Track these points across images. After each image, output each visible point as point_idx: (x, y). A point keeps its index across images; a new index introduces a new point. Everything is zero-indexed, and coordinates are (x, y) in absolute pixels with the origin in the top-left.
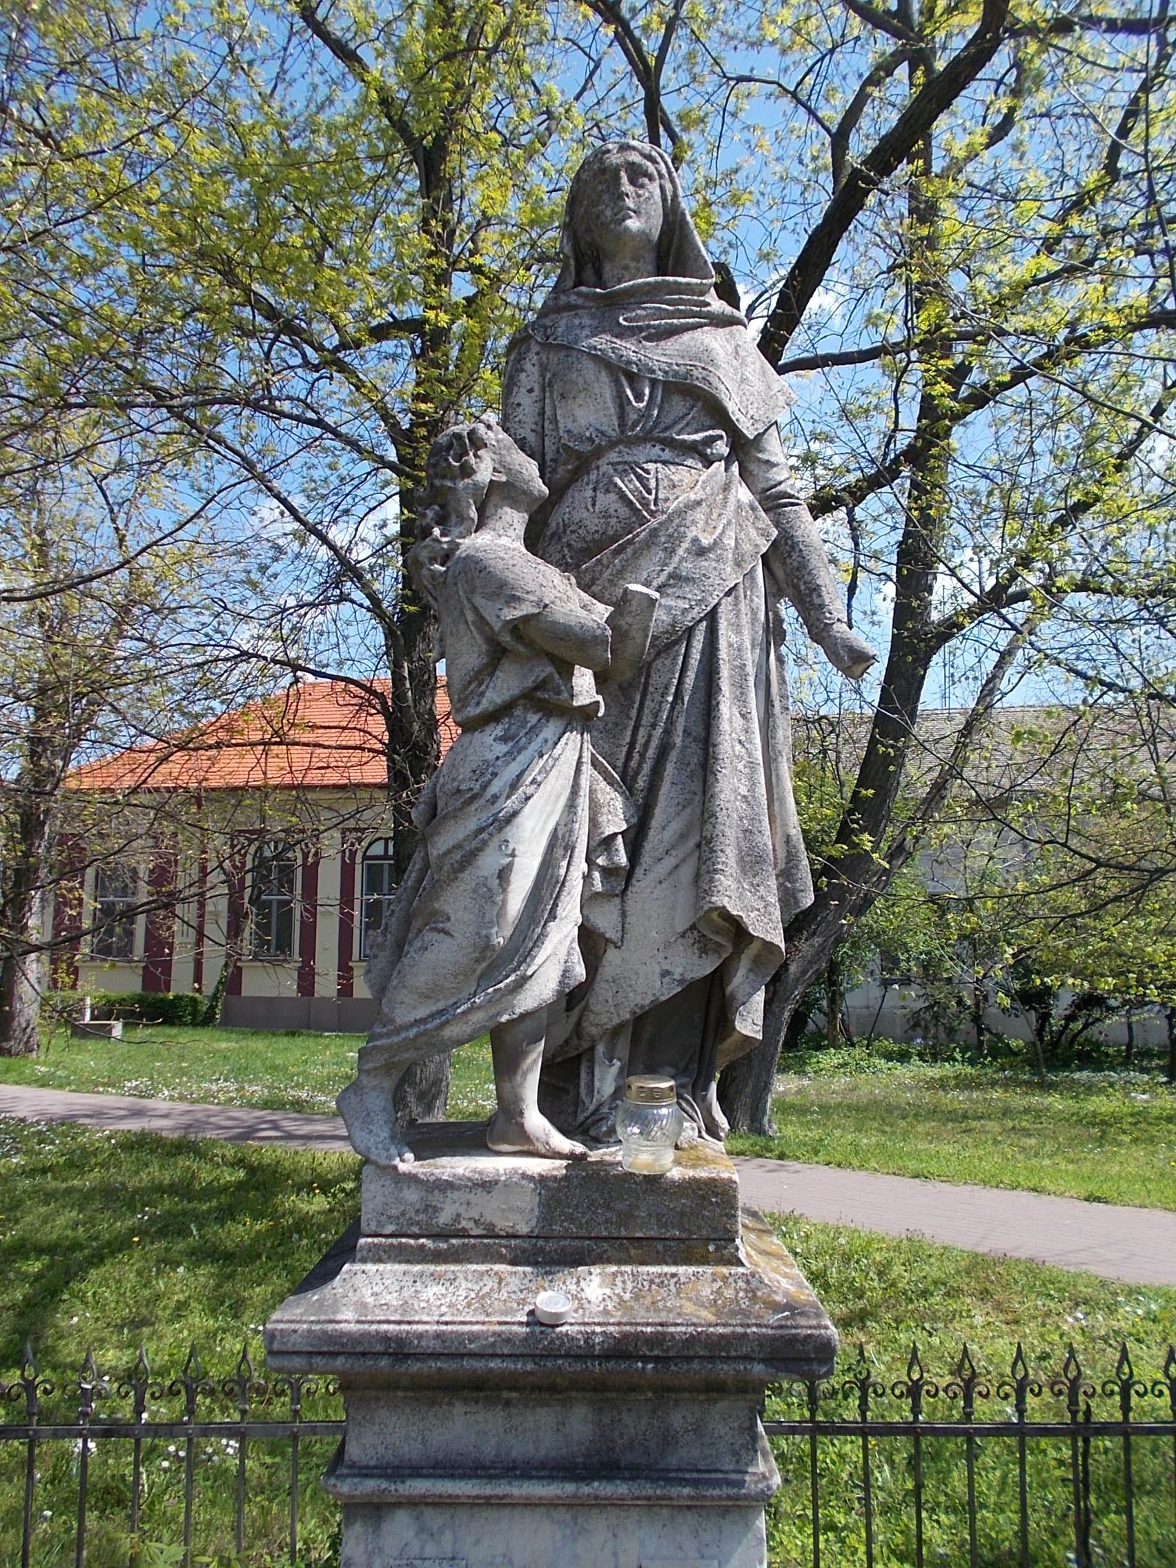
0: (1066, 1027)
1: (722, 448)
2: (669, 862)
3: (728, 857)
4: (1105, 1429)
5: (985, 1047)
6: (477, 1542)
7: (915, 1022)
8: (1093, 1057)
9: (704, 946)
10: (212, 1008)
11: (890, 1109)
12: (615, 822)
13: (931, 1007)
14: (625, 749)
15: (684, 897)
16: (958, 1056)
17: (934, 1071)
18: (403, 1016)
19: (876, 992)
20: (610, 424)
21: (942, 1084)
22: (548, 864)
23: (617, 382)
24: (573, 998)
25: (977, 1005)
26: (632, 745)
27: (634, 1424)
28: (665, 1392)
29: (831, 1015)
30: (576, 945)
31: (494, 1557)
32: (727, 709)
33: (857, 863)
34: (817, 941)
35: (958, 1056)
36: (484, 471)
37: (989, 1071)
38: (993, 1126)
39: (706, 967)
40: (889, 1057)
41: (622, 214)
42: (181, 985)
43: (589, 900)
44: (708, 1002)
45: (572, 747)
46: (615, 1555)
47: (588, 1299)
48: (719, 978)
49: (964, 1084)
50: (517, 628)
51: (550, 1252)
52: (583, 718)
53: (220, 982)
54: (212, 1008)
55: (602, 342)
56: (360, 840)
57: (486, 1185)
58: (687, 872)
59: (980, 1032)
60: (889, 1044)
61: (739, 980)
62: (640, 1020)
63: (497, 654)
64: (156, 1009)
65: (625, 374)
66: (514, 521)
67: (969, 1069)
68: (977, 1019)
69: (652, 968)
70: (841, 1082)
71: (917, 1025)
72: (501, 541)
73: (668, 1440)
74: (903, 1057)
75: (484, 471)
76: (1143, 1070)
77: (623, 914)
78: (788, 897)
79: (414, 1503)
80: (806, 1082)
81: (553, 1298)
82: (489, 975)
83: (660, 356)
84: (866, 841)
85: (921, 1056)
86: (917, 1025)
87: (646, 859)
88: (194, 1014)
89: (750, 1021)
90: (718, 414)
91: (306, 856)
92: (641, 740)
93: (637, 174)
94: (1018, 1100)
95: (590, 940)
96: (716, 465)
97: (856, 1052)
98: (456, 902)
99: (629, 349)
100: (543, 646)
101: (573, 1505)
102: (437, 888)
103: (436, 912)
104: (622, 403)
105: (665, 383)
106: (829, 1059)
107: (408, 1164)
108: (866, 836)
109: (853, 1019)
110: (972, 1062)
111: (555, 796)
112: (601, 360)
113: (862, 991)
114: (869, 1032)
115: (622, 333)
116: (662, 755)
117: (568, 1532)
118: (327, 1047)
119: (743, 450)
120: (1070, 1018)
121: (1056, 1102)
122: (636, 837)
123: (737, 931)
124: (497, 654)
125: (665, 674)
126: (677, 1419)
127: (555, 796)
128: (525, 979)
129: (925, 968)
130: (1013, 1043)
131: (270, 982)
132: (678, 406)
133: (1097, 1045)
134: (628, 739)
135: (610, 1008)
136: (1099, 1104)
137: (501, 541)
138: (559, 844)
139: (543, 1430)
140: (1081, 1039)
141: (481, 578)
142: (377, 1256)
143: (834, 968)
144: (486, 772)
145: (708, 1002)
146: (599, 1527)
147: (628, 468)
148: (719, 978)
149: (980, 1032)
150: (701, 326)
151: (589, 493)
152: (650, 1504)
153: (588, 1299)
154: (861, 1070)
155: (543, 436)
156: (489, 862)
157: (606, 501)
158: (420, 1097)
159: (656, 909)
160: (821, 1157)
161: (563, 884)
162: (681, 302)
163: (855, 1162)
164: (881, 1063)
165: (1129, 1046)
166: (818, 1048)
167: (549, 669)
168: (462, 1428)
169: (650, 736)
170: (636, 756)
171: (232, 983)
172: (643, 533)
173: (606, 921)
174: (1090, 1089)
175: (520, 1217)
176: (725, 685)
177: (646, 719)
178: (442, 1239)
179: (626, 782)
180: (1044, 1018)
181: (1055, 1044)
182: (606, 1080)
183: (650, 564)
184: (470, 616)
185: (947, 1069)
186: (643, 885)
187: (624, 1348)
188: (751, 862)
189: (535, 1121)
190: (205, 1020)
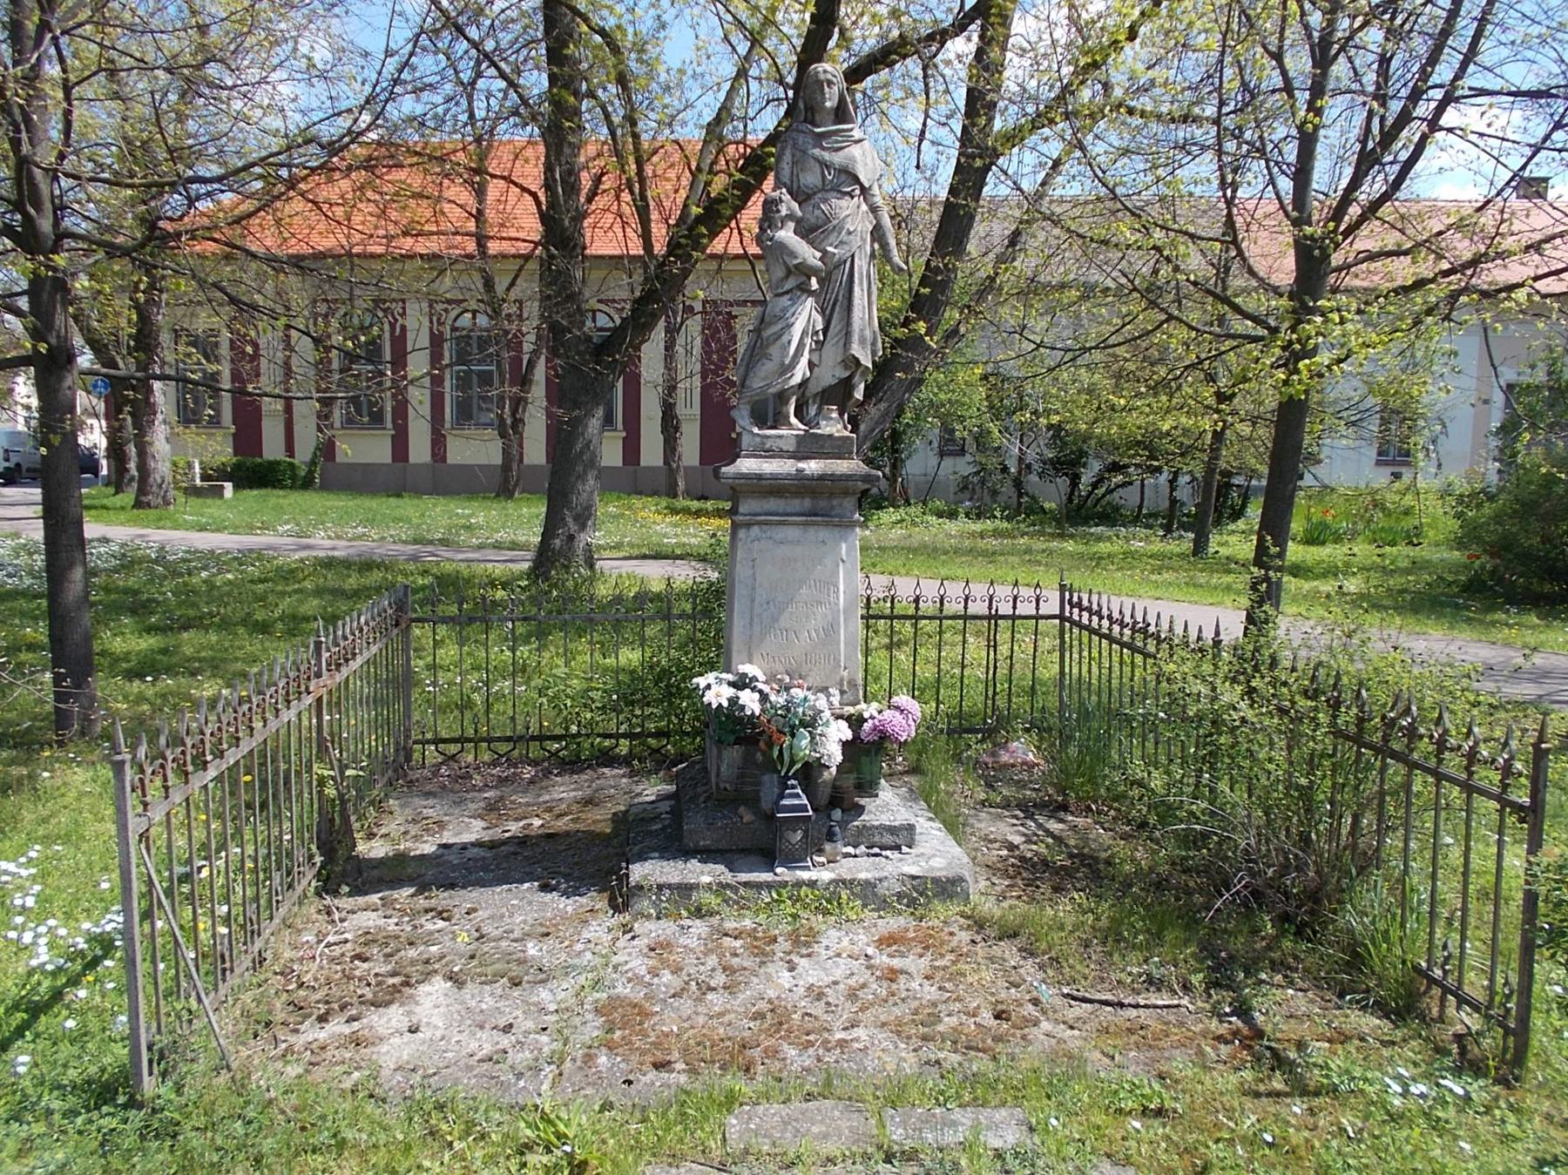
0: (1091, 493)
1: (858, 192)
3: (856, 338)
4: (1004, 617)
5: (1024, 509)
7: (964, 486)
8: (1111, 517)
9: (846, 367)
10: (311, 473)
11: (935, 550)
12: (820, 326)
13: (977, 473)
15: (841, 350)
16: (998, 514)
17: (977, 526)
18: (755, 386)
19: (934, 461)
20: (819, 184)
21: (982, 535)
22: (801, 339)
24: (804, 383)
25: (1020, 472)
27: (823, 504)
28: (832, 495)
29: (892, 479)
32: (856, 288)
33: (915, 343)
34: (883, 406)
35: (998, 514)
36: (784, 212)
37: (1022, 526)
38: (1015, 559)
39: (847, 374)
40: (940, 515)
41: (824, 100)
42: (273, 448)
43: (811, 351)
44: (846, 385)
45: (810, 302)
47: (812, 466)
48: (851, 377)
49: (997, 533)
50: (796, 266)
51: (798, 455)
52: (811, 293)
53: (317, 448)
54: (311, 473)
55: (817, 151)
57: (780, 437)
58: (841, 343)
59: (1020, 495)
60: (939, 504)
61: (857, 378)
62: (824, 391)
63: (789, 273)
64: (254, 473)
65: (825, 165)
66: (791, 225)
67: (1006, 525)
68: (1018, 483)
69: (830, 374)
70: (898, 532)
71: (965, 487)
72: (787, 234)
73: (832, 508)
74: (952, 515)
75: (784, 212)
76: (1148, 527)
78: (874, 353)
79: (759, 523)
80: (868, 533)
81: (801, 465)
82: (783, 373)
83: (837, 159)
84: (922, 327)
85: (967, 516)
86: (965, 487)
88: (294, 477)
89: (859, 394)
90: (857, 180)
91: (393, 326)
93: (830, 83)
94: (1039, 544)
95: (811, 365)
97: (912, 510)
98: (774, 351)
99: (826, 156)
100: (804, 271)
101: (806, 524)
102: (768, 346)
104: (824, 176)
106: (888, 516)
107: (756, 430)
108: (922, 323)
109: (912, 485)
110: (1009, 519)
111: (805, 316)
112: (817, 160)
113: (920, 461)
114: (925, 495)
115: (823, 149)
116: (836, 306)
118: (435, 505)
119: (865, 191)
120: (1095, 486)
121: (1070, 546)
122: (825, 331)
123: (857, 361)
124: (789, 273)
125: (837, 276)
126: (835, 502)
127: (805, 316)
129: (976, 439)
130: (1047, 505)
131: (365, 448)
132: (843, 177)
133: (1117, 509)
135: (814, 388)
136: (1104, 548)
137: (787, 234)
138: (804, 333)
139: (796, 504)
140: (1103, 502)
141: (782, 247)
142: (747, 456)
143: (896, 436)
144: (785, 310)
145: (846, 385)
146: (812, 530)
147: (825, 201)
148: (851, 377)
149: (1020, 495)
152: (827, 524)
153: (812, 466)
154: (914, 524)
156: (785, 338)
157: (817, 212)
158: (576, 518)
159: (832, 354)
160: (878, 569)
163: (903, 571)
164: (933, 519)
165: (1140, 507)
166: (880, 507)
168: (773, 504)
171: (327, 450)
172: (830, 226)
174: (1099, 539)
175: (790, 446)
176: (856, 280)
178: (770, 454)
179: (823, 313)
180: (1075, 479)
181: (1080, 507)
182: (813, 411)
183: (832, 238)
185: (988, 524)
186: (827, 346)
187: (822, 477)
188: (862, 341)
189: (793, 420)
190: (307, 484)
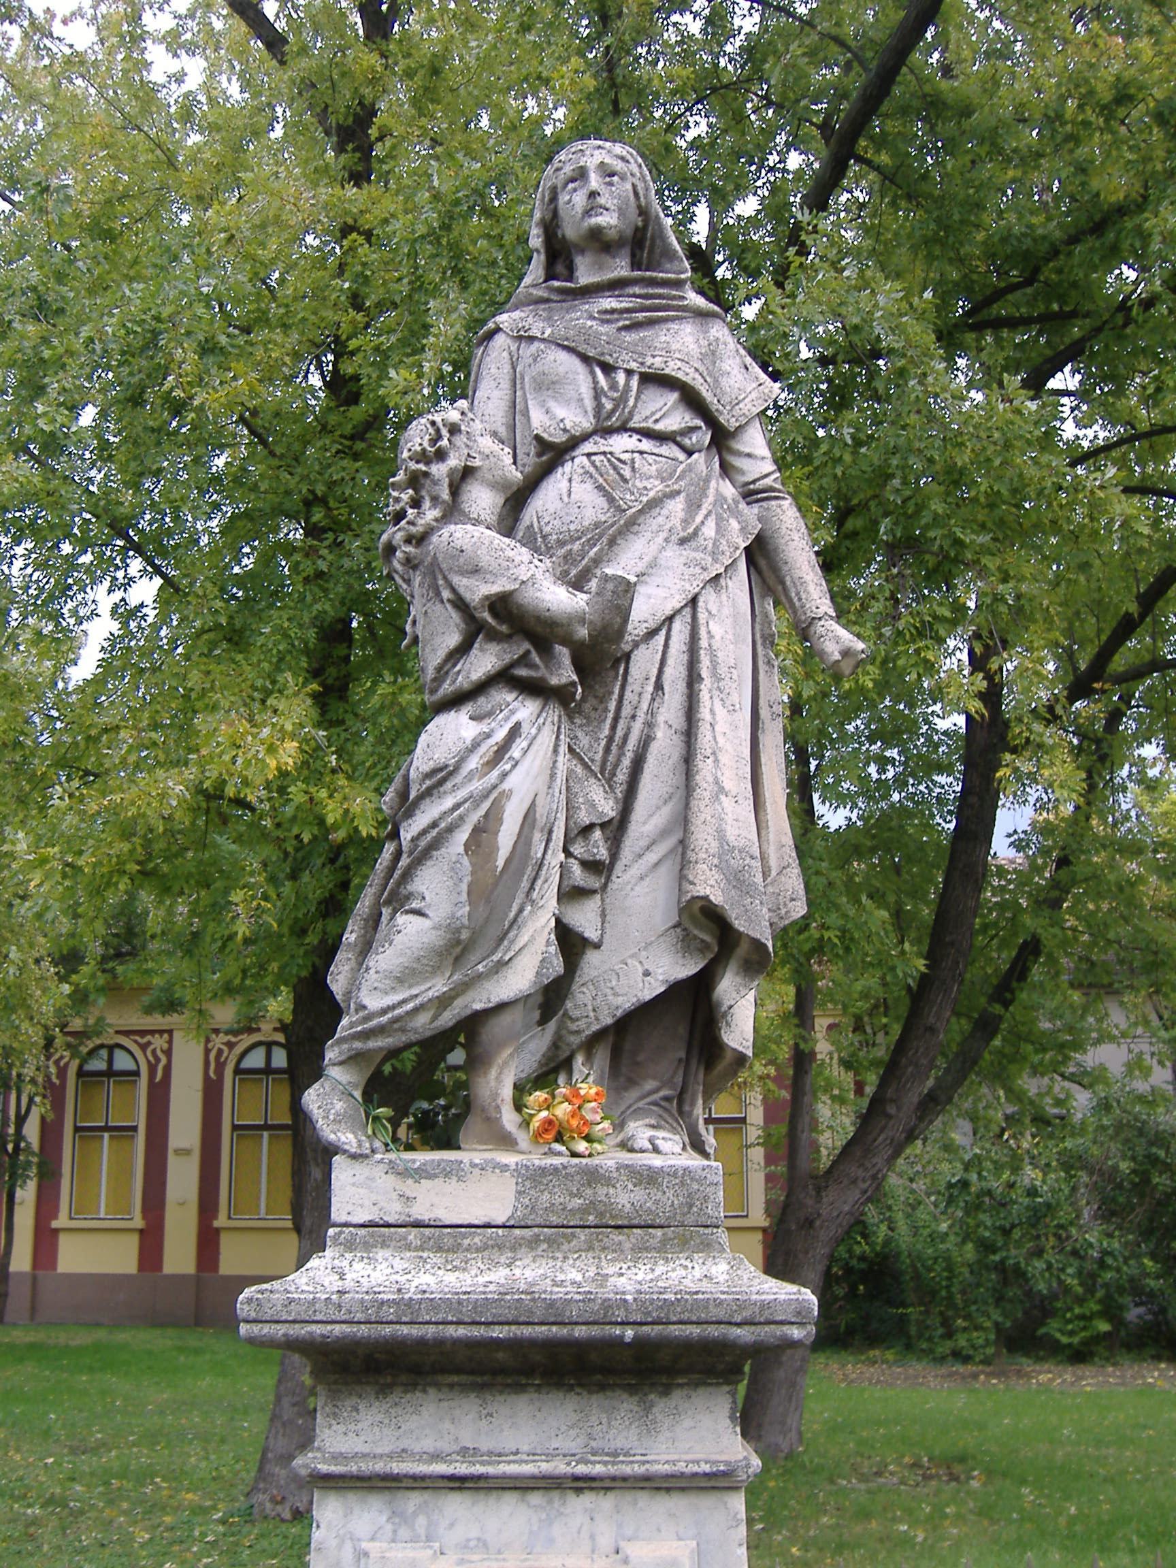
2: (652, 857)
6: (452, 1525)
14: (603, 743)
23: (593, 373)
26: (610, 739)
30: (553, 937)
31: (469, 1540)
39: (687, 969)
46: (592, 1537)
56: (231, 1045)
77: (603, 915)
87: (626, 853)
92: (620, 733)
96: (695, 456)
103: (411, 894)
105: (641, 374)
117: (544, 1516)
128: (502, 965)
134: (606, 732)
145: (692, 1005)
150: (682, 318)
151: (564, 485)
155: (513, 428)
161: (541, 865)
162: (660, 297)
167: (526, 645)
169: (629, 729)
170: (614, 748)
173: (584, 918)
177: (626, 711)
184: (446, 594)
